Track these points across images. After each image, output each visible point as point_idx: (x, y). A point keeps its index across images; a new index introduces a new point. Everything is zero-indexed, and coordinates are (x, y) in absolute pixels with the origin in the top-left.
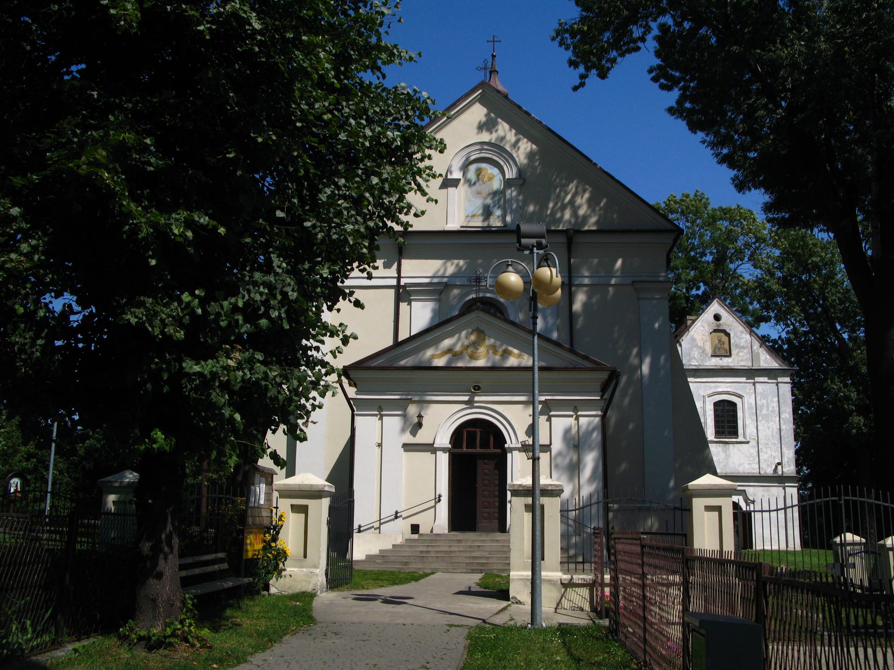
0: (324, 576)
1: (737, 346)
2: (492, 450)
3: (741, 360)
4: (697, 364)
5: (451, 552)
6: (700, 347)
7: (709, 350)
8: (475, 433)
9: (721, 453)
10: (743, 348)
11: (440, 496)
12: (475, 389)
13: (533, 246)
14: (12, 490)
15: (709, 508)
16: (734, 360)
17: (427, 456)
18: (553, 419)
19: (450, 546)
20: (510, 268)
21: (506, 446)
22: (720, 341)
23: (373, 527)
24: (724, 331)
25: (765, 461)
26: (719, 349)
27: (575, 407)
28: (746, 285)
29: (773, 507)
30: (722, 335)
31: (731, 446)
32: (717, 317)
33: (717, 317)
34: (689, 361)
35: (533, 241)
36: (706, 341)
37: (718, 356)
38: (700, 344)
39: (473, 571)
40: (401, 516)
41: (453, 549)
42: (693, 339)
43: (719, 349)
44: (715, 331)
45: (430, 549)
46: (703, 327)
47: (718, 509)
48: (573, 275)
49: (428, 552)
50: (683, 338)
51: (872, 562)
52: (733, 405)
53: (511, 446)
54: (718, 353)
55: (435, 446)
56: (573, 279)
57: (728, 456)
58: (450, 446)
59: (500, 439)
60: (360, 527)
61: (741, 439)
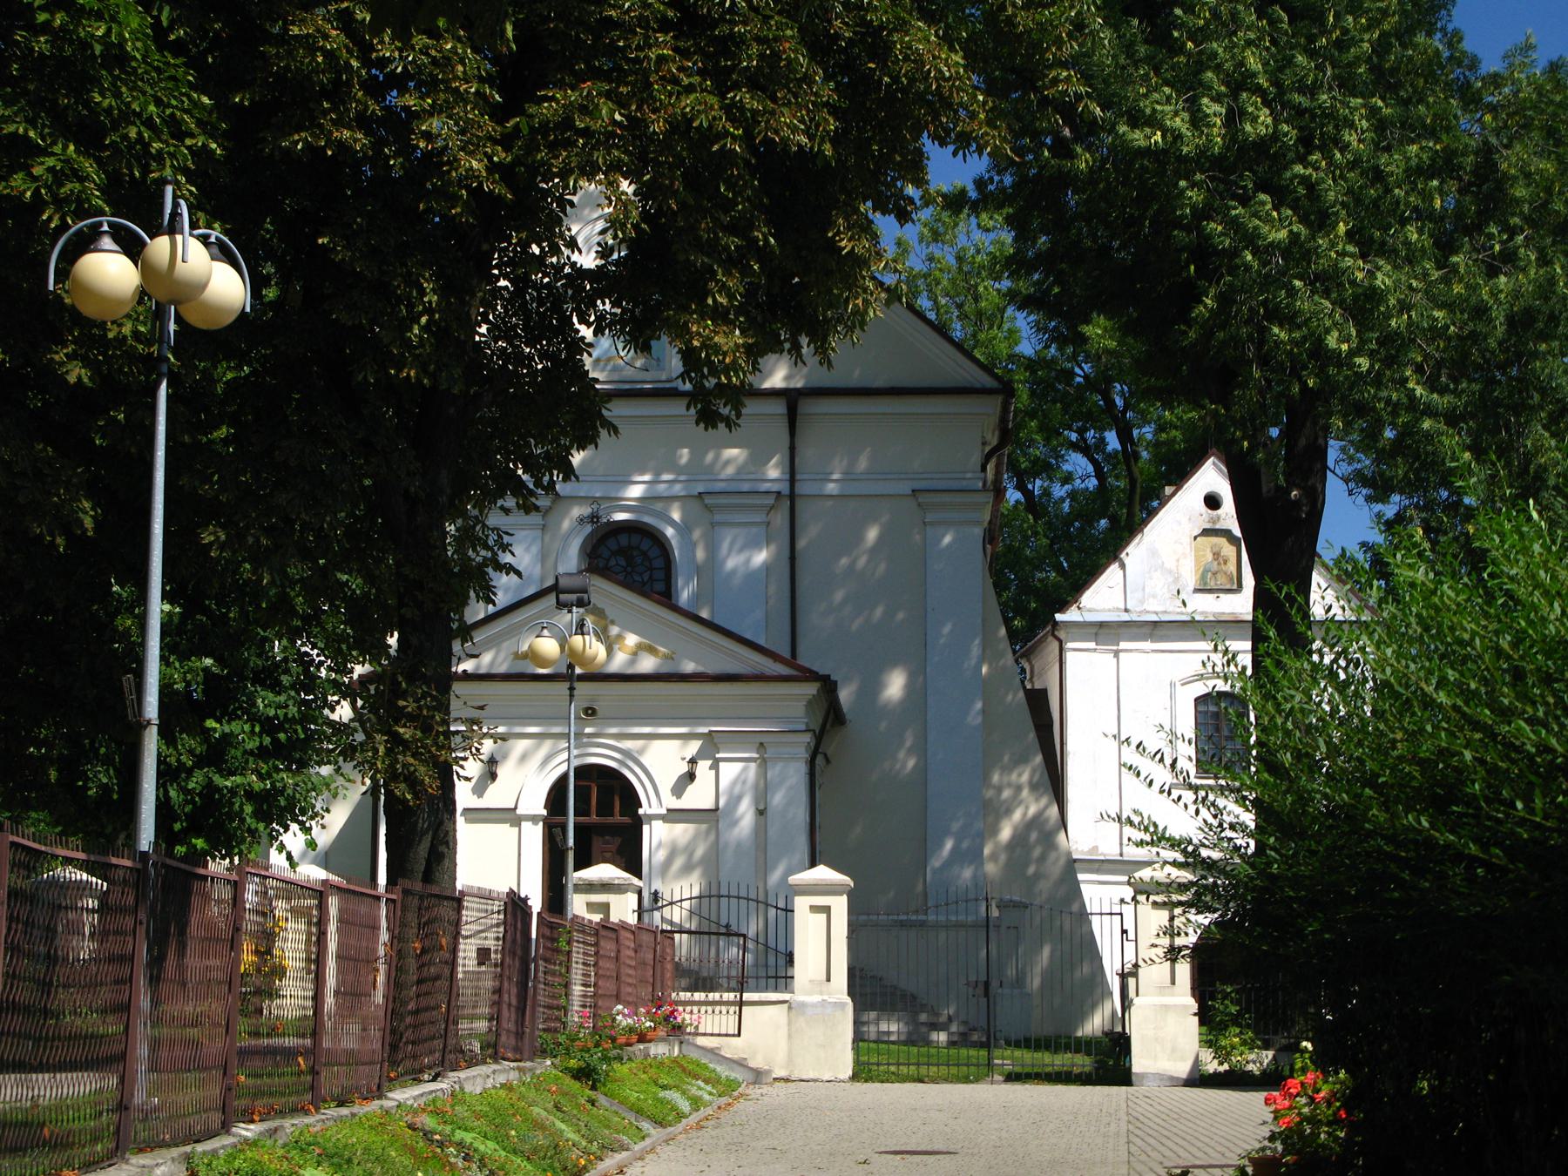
2: (618, 818)
4: (1159, 609)
6: (1170, 572)
7: (1190, 580)
8: (589, 788)
12: (587, 714)
15: (815, 909)
17: (505, 831)
18: (722, 765)
20: (546, 632)
21: (641, 811)
22: (1216, 555)
26: (1214, 574)
27: (761, 744)
29: (724, 901)
30: (1222, 541)
34: (1142, 602)
35: (573, 597)
37: (1210, 591)
42: (1154, 553)
43: (1214, 574)
44: (1206, 532)
47: (826, 910)
48: (798, 477)
50: (1130, 549)
53: (649, 812)
54: (1212, 584)
55: (518, 812)
56: (797, 485)
58: (545, 812)
59: (631, 799)
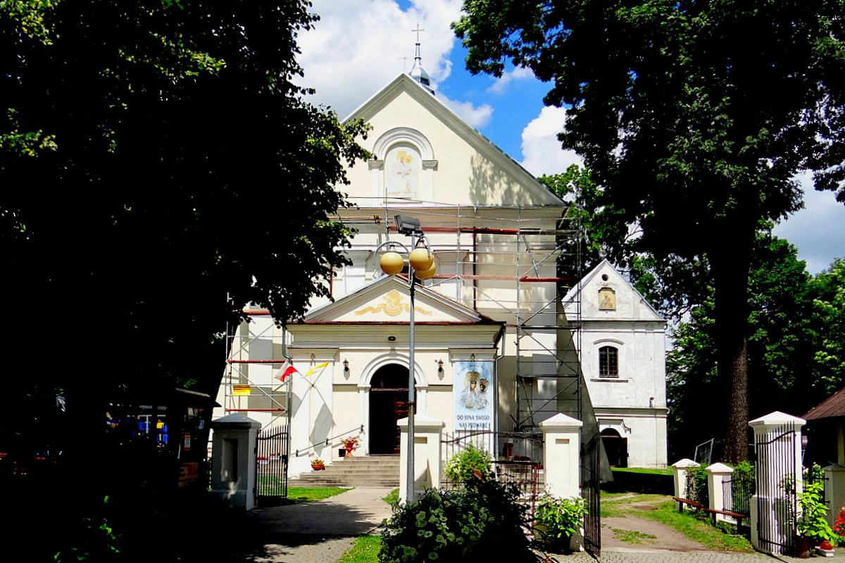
0: (252, 494)
1: (620, 301)
3: (624, 314)
5: (368, 471)
6: (589, 303)
7: (597, 306)
10: (626, 303)
11: (362, 426)
13: (412, 230)
19: (368, 467)
23: (308, 453)
24: (610, 289)
28: (819, 120)
31: (612, 384)
32: (605, 278)
33: (605, 278)
37: (604, 310)
38: (590, 300)
40: (331, 444)
41: (371, 469)
45: (352, 469)
49: (351, 472)
51: (500, 345)
52: (615, 350)
53: (420, 386)
58: (370, 386)
60: (297, 452)
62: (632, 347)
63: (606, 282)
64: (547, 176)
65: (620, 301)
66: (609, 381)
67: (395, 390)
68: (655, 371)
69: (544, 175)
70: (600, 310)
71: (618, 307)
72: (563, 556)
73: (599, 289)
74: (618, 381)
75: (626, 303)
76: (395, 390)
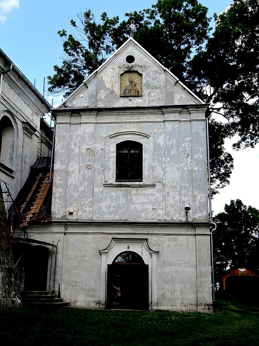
1: (148, 86)
6: (108, 89)
7: (117, 91)
9: (121, 197)
10: (156, 88)
14: (16, 273)
16: (144, 100)
25: (172, 206)
33: (130, 59)
36: (116, 83)
38: (108, 86)
39: (157, 299)
42: (102, 82)
46: (114, 69)
52: (139, 146)
57: (129, 201)
61: (145, 182)
62: (161, 140)
63: (130, 65)
64: (60, 65)
65: (148, 86)
66: (128, 186)
67: (42, 245)
68: (192, 171)
69: (56, 68)
70: (121, 97)
71: (145, 92)
72: (53, 207)
73: (122, 72)
74: (140, 186)
75: (156, 88)
76: (42, 245)
